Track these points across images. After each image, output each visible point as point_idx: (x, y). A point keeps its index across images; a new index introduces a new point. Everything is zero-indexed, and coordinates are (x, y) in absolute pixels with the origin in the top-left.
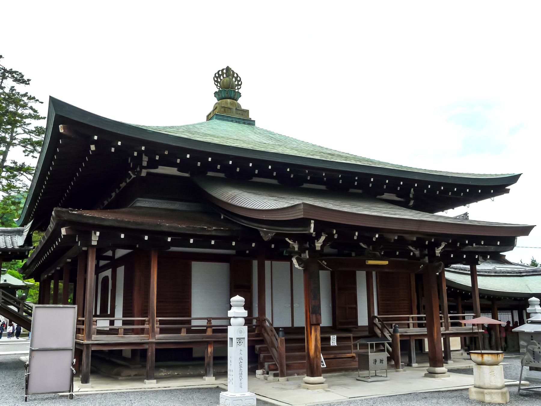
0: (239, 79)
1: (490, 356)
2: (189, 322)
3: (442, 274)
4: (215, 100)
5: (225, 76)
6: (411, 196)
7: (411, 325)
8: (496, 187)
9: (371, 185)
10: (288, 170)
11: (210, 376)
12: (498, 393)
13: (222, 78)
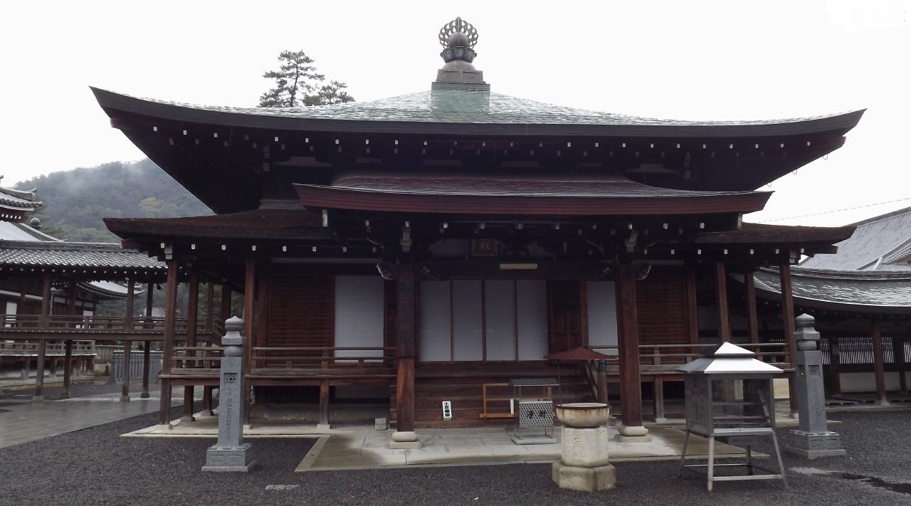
0: (473, 31)
1: (573, 412)
2: (331, 353)
3: (749, 281)
4: (442, 64)
5: (454, 30)
6: (687, 165)
7: (657, 360)
8: (816, 139)
9: (396, 151)
10: (757, 146)
11: (324, 423)
12: (580, 475)
13: (450, 33)
